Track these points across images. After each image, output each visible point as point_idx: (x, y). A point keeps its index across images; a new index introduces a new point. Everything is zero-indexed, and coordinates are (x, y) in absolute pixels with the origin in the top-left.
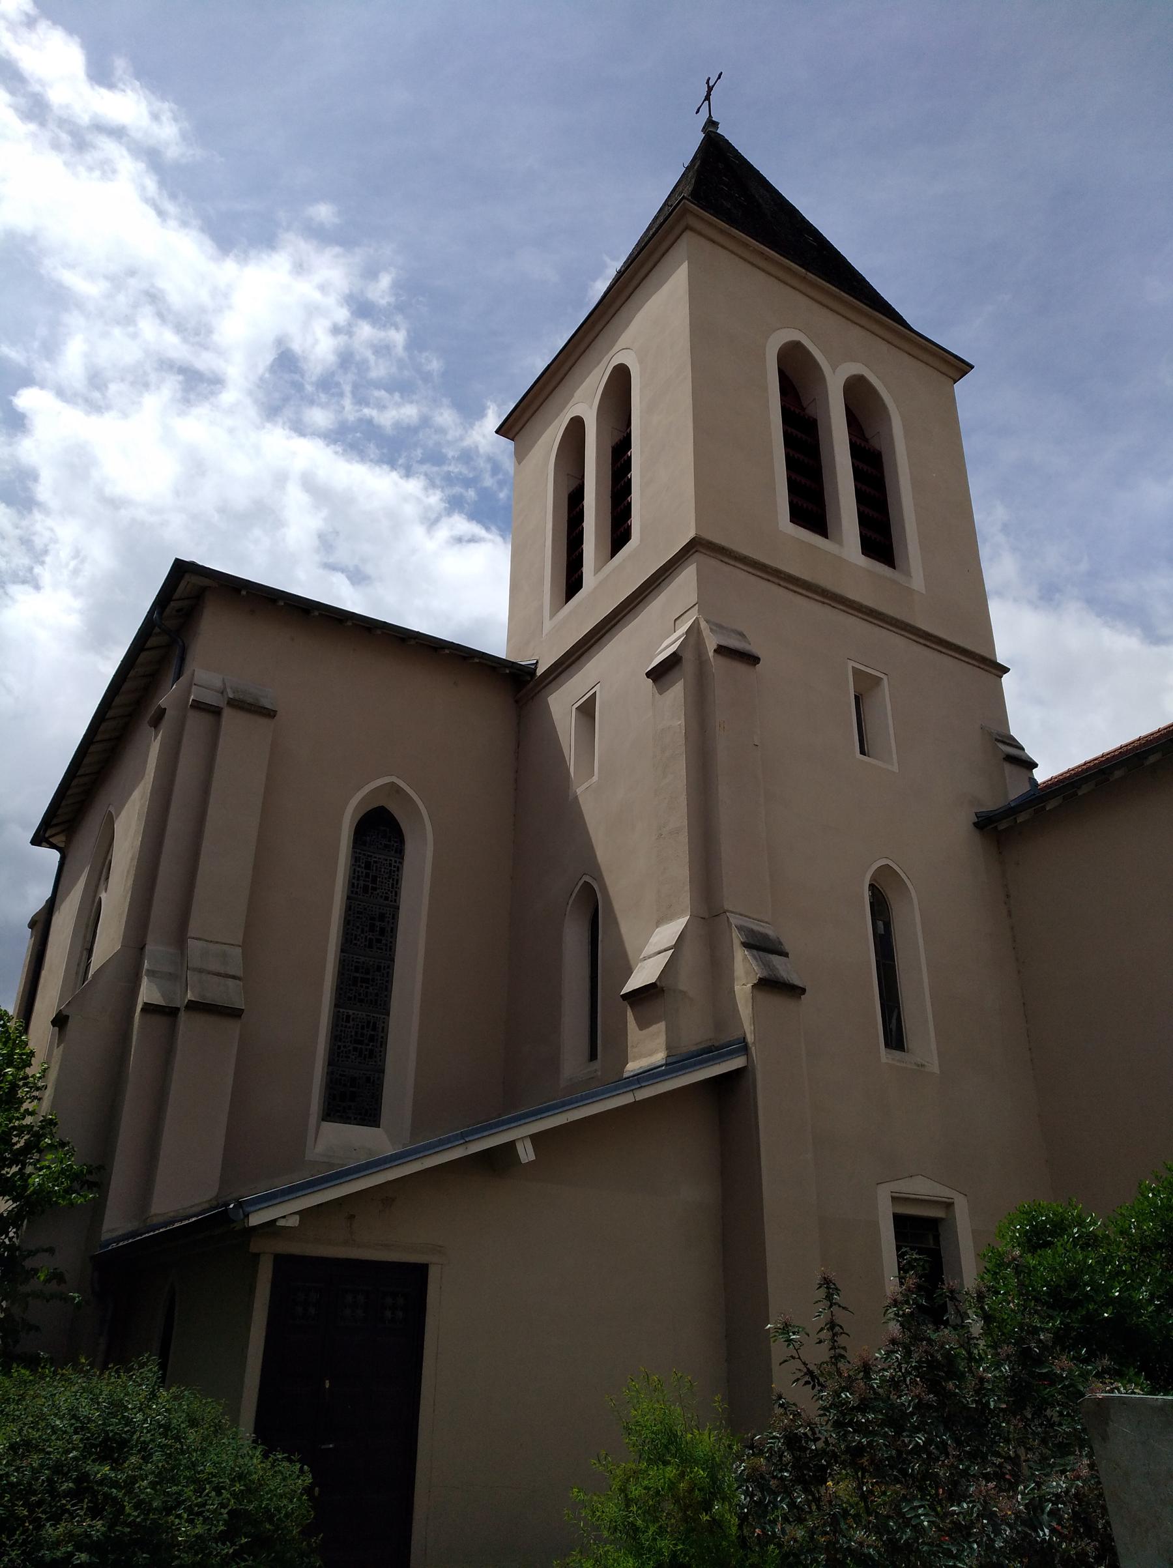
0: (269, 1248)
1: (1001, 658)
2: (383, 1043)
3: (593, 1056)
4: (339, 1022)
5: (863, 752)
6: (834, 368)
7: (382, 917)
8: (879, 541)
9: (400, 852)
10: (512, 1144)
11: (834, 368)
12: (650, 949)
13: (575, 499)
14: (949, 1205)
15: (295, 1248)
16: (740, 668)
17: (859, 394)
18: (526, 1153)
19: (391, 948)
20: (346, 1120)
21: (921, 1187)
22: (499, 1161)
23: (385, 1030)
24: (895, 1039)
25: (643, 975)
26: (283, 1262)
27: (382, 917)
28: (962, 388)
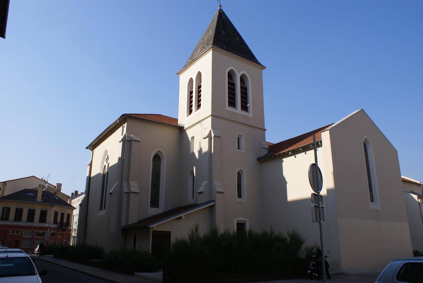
0: (151, 230)
1: (266, 128)
2: (159, 195)
3: (193, 198)
4: (152, 191)
5: (239, 148)
6: (238, 73)
7: (158, 174)
8: (245, 108)
9: (160, 162)
10: (182, 216)
11: (238, 73)
12: (202, 185)
13: (191, 93)
14: (246, 221)
15: (154, 230)
16: (201, 195)
17: (243, 79)
18: (184, 217)
19: (159, 178)
20: (154, 207)
21: (241, 219)
22: (181, 218)
23: (159, 192)
24: (240, 196)
25: (200, 190)
26: (153, 231)
27: (158, 174)
28: (264, 71)
